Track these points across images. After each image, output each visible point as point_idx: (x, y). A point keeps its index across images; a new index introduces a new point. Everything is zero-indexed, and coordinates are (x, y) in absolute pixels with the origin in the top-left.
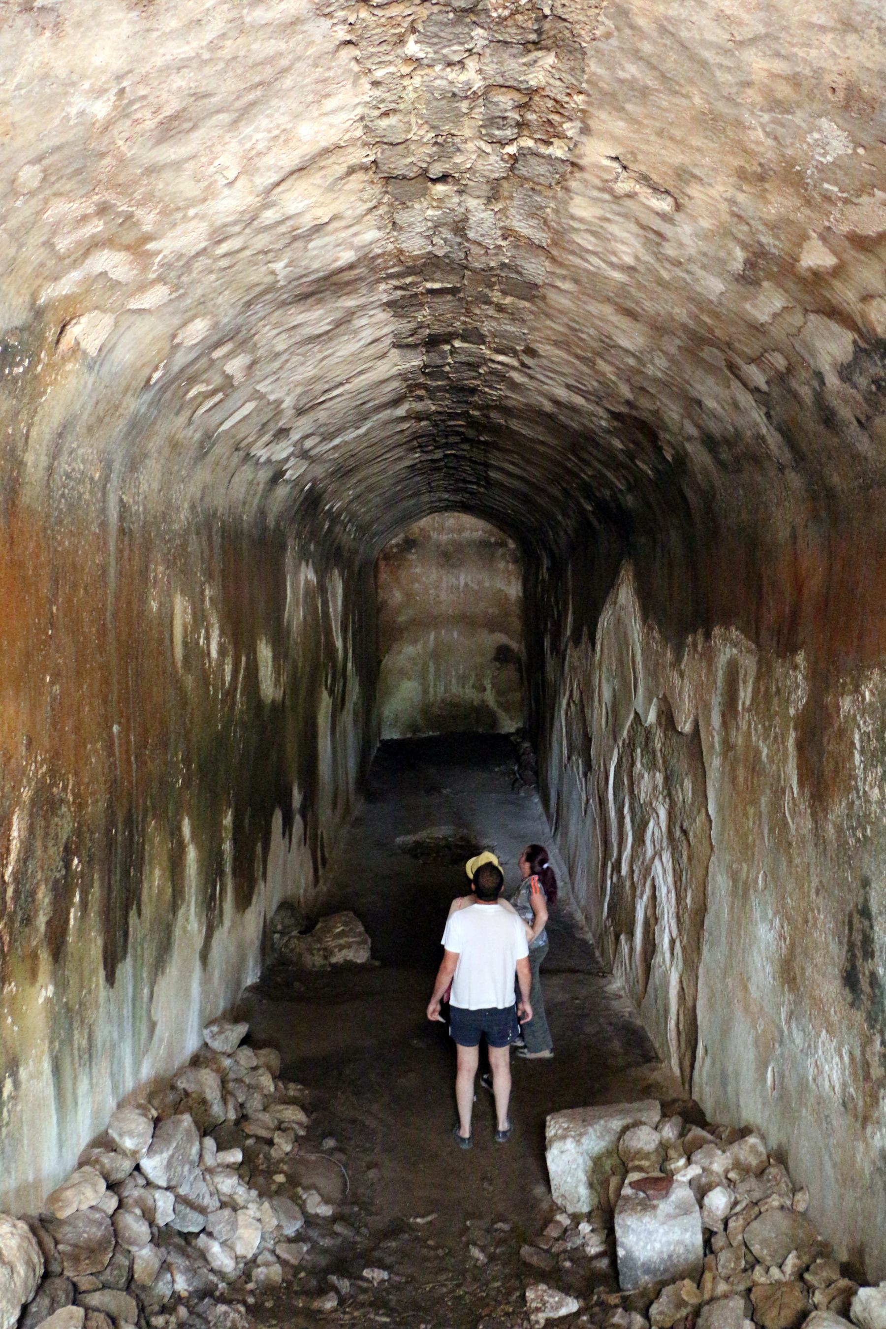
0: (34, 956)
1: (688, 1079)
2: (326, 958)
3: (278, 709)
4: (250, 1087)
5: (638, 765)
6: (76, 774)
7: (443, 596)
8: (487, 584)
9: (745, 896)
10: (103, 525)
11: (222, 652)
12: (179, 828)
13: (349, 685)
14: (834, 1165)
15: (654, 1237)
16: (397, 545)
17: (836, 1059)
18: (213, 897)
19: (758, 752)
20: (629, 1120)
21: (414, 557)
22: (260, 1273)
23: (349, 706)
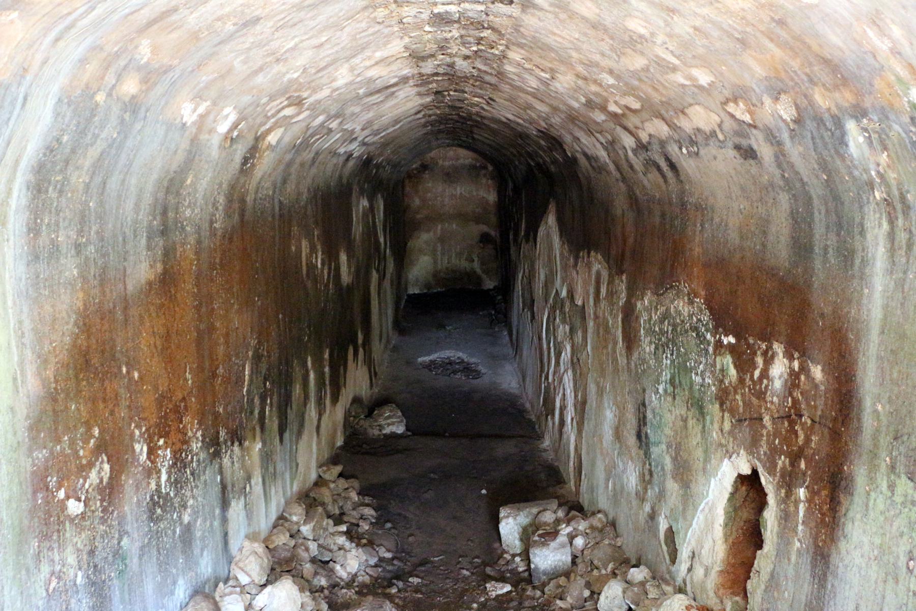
0: (254, 429)
1: (578, 492)
2: (380, 430)
3: (350, 288)
4: (345, 498)
5: (558, 320)
10: (273, 216)
11: (323, 264)
12: (306, 362)
13: (388, 264)
16: (416, 169)
19: (608, 322)
20: (541, 509)
22: (360, 579)
23: (388, 276)
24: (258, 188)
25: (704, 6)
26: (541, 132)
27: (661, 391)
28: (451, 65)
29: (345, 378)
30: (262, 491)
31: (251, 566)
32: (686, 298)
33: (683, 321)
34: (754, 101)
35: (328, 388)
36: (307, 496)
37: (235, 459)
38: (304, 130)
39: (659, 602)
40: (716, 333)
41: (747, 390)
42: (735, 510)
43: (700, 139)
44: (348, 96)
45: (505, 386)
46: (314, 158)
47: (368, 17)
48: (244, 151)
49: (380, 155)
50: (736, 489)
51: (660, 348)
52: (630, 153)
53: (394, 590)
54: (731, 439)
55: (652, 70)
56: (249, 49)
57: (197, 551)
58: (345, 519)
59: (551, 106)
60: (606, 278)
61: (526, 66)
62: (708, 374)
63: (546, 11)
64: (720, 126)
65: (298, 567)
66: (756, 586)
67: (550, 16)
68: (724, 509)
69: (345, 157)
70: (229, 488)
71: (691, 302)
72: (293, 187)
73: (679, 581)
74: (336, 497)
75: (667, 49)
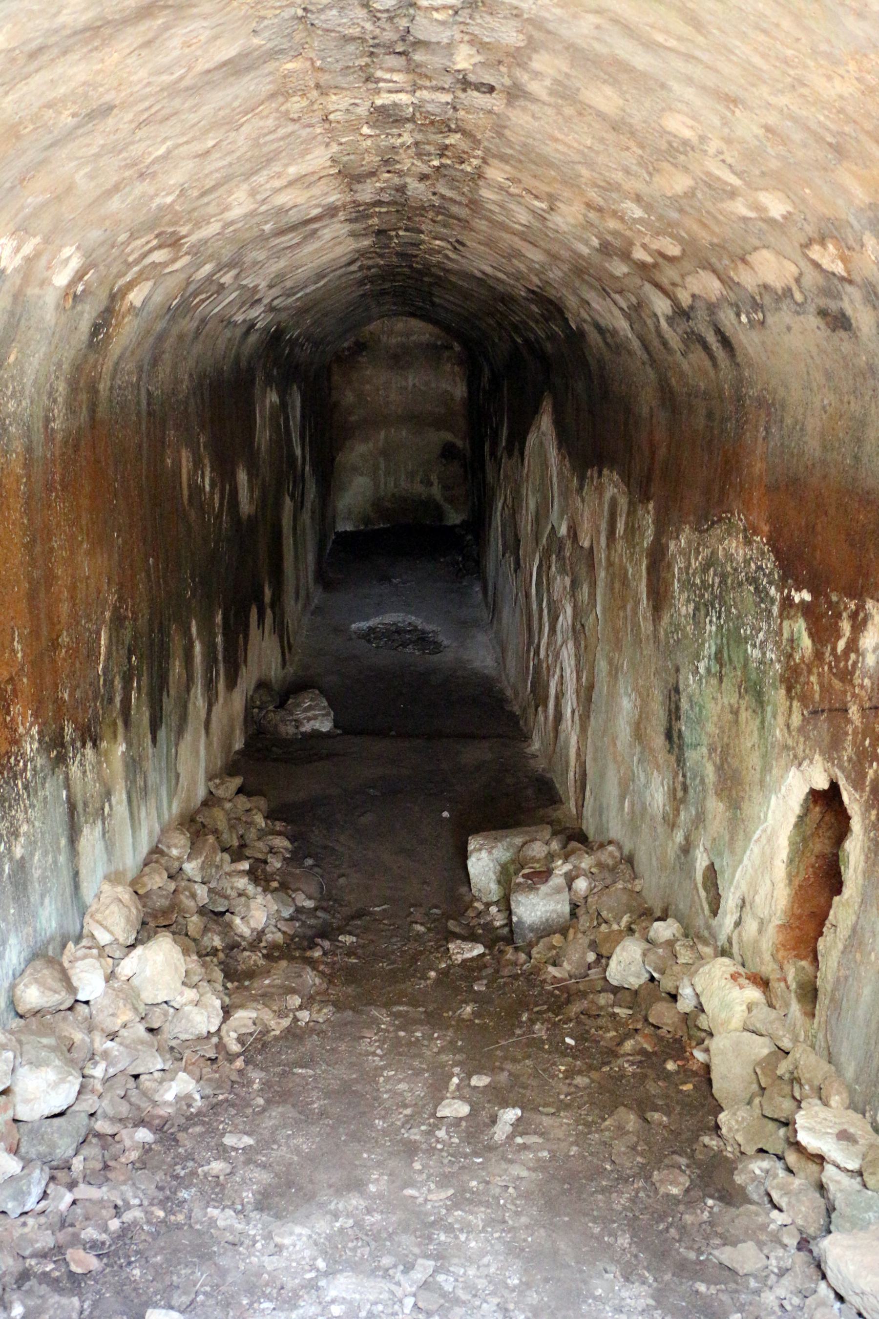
0: (115, 724)
1: (580, 815)
2: (297, 727)
3: (253, 520)
5: (553, 569)
6: (132, 598)
7: (393, 397)
8: (433, 385)
9: (616, 677)
11: (212, 485)
12: (189, 628)
13: (307, 486)
14: (657, 859)
15: (535, 908)
16: (349, 349)
17: (661, 789)
18: (211, 680)
20: (528, 838)
21: (365, 359)
22: (269, 937)
23: (308, 505)
24: (115, 370)
25: (782, 92)
26: (533, 292)
27: (702, 670)
28: (401, 189)
29: (246, 650)
30: (127, 814)
31: (113, 920)
32: (741, 536)
33: (736, 570)
34: (851, 242)
35: (221, 666)
36: (192, 820)
37: (88, 768)
38: (184, 285)
39: (693, 969)
40: (784, 587)
41: (826, 668)
42: (804, 840)
43: (767, 300)
44: (248, 235)
45: (477, 664)
46: (198, 328)
47: (277, 110)
48: (94, 314)
49: (297, 325)
50: (806, 811)
51: (702, 607)
52: (663, 323)
53: (317, 954)
54: (802, 739)
55: (700, 195)
56: (98, 156)
57: (34, 898)
58: (248, 852)
59: (548, 252)
60: (625, 508)
61: (512, 190)
62: (770, 646)
63: (544, 103)
64: (798, 281)
65: (181, 920)
66: (831, 946)
67: (550, 111)
68: (789, 838)
69: (244, 330)
70: (80, 807)
71: (748, 542)
72: (168, 370)
73: (722, 939)
74: (234, 822)
75: (723, 161)
